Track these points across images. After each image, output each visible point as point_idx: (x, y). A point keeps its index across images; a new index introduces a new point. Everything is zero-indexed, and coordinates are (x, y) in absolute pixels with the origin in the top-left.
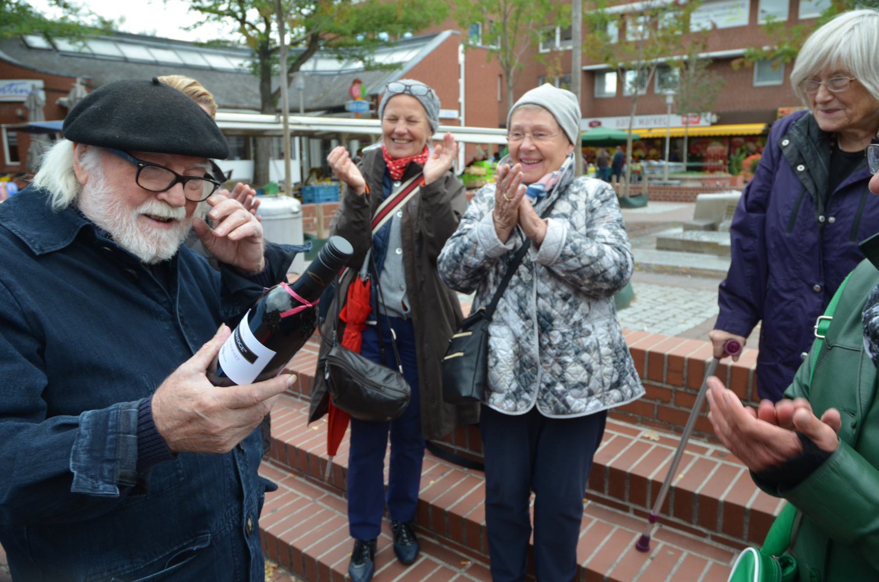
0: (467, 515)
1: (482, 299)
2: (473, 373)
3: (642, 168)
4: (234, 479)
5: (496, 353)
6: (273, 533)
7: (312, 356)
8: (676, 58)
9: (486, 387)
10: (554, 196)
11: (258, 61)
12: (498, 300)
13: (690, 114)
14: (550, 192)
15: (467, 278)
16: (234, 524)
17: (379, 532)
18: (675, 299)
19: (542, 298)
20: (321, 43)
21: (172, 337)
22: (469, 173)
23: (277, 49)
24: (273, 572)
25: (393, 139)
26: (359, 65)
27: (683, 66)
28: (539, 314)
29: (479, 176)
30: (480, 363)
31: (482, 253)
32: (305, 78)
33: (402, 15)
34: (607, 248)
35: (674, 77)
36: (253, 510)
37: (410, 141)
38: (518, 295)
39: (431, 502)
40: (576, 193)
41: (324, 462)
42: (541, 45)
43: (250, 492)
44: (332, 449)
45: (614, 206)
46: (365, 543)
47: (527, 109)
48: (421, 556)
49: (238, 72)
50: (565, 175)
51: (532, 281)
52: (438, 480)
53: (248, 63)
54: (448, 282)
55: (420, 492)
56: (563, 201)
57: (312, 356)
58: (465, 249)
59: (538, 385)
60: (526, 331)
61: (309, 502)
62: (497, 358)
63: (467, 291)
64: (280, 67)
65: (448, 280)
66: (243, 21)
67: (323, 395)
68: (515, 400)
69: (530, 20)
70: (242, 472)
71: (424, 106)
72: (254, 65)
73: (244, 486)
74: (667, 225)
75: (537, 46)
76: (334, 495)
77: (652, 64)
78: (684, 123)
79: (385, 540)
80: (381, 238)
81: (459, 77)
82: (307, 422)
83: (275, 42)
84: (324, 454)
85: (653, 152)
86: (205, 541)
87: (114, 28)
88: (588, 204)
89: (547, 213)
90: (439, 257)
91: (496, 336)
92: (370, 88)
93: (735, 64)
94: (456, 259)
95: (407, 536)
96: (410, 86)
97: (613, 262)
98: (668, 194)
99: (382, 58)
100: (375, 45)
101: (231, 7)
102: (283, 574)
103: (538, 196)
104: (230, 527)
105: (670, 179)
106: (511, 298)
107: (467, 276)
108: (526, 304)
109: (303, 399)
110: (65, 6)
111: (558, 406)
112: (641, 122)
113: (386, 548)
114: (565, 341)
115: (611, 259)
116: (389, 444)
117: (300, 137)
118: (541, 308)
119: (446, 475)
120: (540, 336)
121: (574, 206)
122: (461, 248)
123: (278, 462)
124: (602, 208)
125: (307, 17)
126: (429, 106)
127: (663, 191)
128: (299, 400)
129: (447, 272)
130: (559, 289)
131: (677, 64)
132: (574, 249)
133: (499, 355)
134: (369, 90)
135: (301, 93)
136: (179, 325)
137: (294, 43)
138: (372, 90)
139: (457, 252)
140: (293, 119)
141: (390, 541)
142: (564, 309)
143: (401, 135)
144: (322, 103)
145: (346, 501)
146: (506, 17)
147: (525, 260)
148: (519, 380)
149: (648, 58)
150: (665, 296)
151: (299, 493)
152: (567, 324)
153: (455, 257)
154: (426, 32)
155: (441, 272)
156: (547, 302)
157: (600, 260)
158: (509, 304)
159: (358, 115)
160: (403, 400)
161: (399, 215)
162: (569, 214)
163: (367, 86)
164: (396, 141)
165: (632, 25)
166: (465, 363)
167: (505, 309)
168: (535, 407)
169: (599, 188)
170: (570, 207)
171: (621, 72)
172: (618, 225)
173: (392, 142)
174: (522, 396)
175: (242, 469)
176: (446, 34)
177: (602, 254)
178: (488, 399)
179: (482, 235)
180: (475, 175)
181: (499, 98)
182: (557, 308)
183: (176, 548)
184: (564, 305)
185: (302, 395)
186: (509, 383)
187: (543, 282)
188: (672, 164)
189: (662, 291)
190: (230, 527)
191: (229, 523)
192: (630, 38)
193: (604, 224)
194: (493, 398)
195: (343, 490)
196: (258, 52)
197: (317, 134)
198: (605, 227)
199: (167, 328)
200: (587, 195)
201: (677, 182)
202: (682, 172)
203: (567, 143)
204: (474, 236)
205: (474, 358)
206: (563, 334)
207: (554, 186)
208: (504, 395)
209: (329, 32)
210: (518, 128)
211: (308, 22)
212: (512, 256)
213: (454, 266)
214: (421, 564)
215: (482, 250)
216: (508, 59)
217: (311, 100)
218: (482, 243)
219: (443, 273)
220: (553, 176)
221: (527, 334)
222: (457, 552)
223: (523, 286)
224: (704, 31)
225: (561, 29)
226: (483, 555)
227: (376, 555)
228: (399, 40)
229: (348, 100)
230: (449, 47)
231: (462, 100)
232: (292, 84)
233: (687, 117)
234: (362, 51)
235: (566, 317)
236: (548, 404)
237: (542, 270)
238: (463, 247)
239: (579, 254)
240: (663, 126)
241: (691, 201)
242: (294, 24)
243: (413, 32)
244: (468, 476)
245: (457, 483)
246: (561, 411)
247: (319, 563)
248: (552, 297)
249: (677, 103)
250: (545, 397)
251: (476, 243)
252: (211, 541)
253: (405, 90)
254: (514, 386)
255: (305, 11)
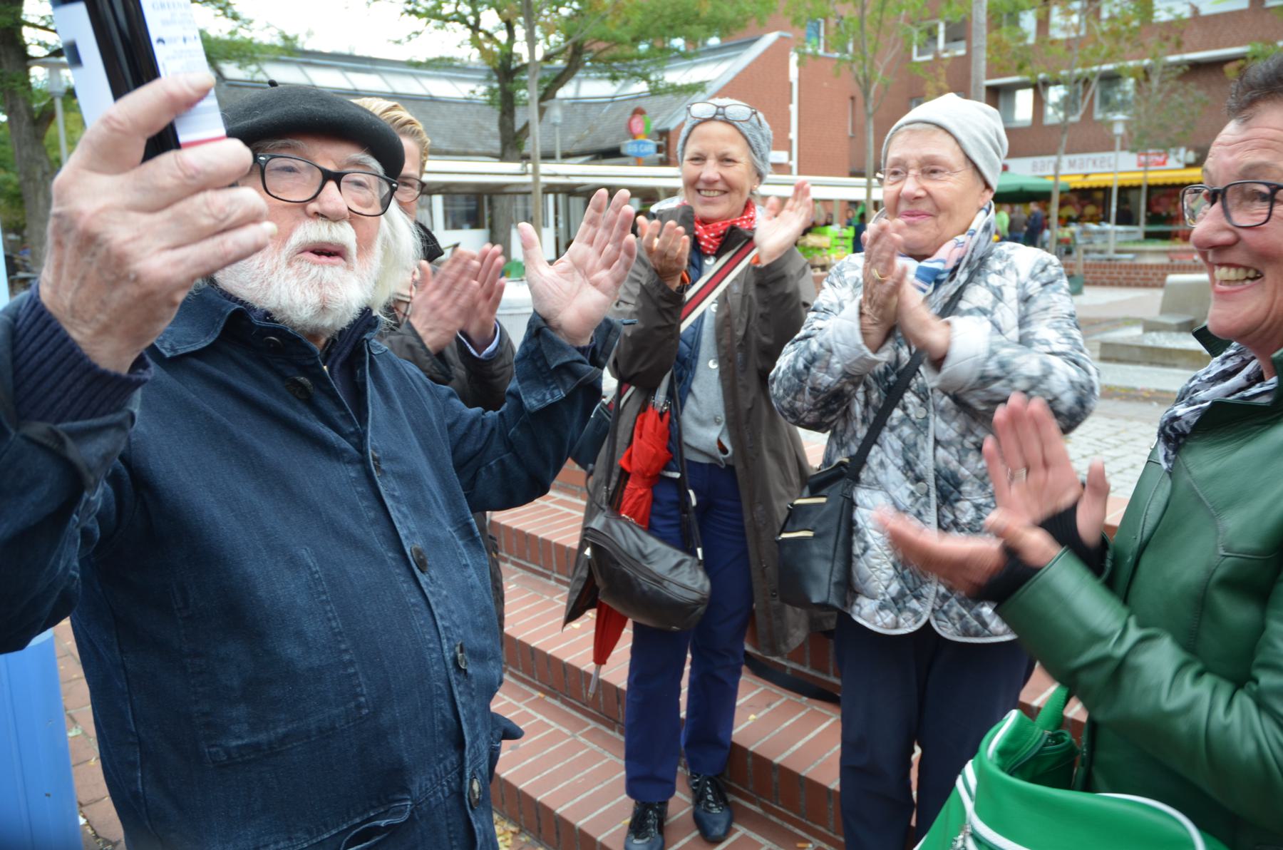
0: (807, 771)
1: (842, 445)
2: (829, 565)
3: (1073, 234)
4: (449, 715)
5: (864, 535)
6: (513, 781)
7: (572, 518)
8: (1131, 63)
9: (849, 587)
10: (962, 277)
11: (496, 85)
12: (869, 449)
13: (1150, 151)
14: (955, 269)
15: (815, 408)
16: (450, 787)
17: (672, 793)
18: (1132, 440)
19: (943, 447)
20: (586, 57)
21: (359, 489)
22: (804, 245)
23: (524, 67)
24: (512, 839)
25: (699, 191)
26: (641, 87)
27: (1141, 76)
28: (938, 474)
29: (820, 249)
30: (840, 548)
31: (838, 366)
32: (564, 108)
33: (706, 10)
34: (1056, 362)
35: (1125, 93)
36: (481, 767)
37: (725, 192)
38: (904, 442)
39: (751, 749)
40: (1000, 273)
41: (587, 676)
42: (915, 50)
43: (476, 738)
44: (602, 654)
45: (1063, 291)
46: (651, 806)
47: (912, 131)
48: (736, 831)
49: (468, 102)
50: (978, 241)
51: (926, 418)
52: (762, 714)
53: (483, 89)
54: (786, 414)
55: (735, 732)
56: (978, 287)
57: (572, 518)
58: (812, 361)
59: (934, 588)
60: (917, 500)
61: (566, 736)
62: (866, 542)
63: (816, 426)
64: (527, 94)
65: (787, 410)
66: (475, 28)
67: (583, 584)
68: (896, 610)
69: (901, 11)
70: (464, 705)
71: (746, 138)
72: (491, 91)
73: (465, 727)
74: (1115, 323)
75: (909, 51)
76: (602, 727)
77: (1094, 74)
78: (1140, 165)
79: (680, 804)
80: (687, 344)
81: (791, 102)
82: (562, 618)
83: (520, 58)
84: (589, 666)
85: (1090, 210)
86: (401, 812)
87: (299, 45)
88: (1021, 290)
89: (950, 308)
90: (772, 373)
91: (865, 506)
92: (656, 121)
93: (1230, 69)
94: (797, 375)
95: (714, 797)
96: (724, 108)
97: (1068, 385)
98: (1115, 275)
99: (676, 76)
100: (665, 56)
101: (460, 9)
102: (526, 842)
103: (935, 279)
104: (443, 792)
105: (1118, 252)
106: (892, 447)
107: (815, 405)
108: (918, 457)
109: (558, 580)
110: (235, 17)
111: (967, 622)
112: (1072, 164)
113: (681, 814)
114: (981, 518)
115: (1064, 379)
116: (689, 656)
117: (556, 193)
118: (942, 465)
119: (773, 707)
120: (938, 509)
121: (998, 294)
122: (806, 359)
123: (520, 674)
124: (1043, 295)
125: (569, 19)
126: (754, 137)
127: (1107, 270)
128: (553, 583)
129: (784, 398)
130: (972, 433)
131: (1133, 72)
132: (1002, 365)
133: (869, 539)
134: (656, 124)
135: (557, 129)
136: (370, 471)
137: (548, 58)
138: (659, 124)
139: (800, 365)
140: (545, 167)
141: (688, 805)
142: (980, 466)
143: (710, 183)
144: (587, 145)
145: (622, 739)
146: (863, 8)
147: (914, 384)
148: (903, 578)
149: (1086, 64)
150: (1117, 434)
151: (552, 723)
152: (984, 490)
153: (797, 374)
154: (739, 36)
155: (775, 396)
156: (950, 453)
157: (1046, 381)
158: (887, 456)
159: (639, 161)
160: (697, 603)
161: (714, 308)
162: (989, 308)
163: (656, 116)
164: (703, 193)
165: (1061, 14)
166: (816, 550)
167: (882, 464)
168: (928, 623)
169: (1037, 263)
170: (991, 297)
171: (1039, 89)
172: (1071, 322)
173: (697, 193)
174: (908, 605)
175: (463, 699)
176: (770, 38)
177: (1047, 372)
178: (852, 604)
179: (839, 338)
180: (812, 248)
181: (850, 133)
182: (967, 466)
183: (358, 820)
184: (979, 460)
185: (556, 575)
186: (885, 583)
187: (945, 421)
188: (1121, 228)
189: (1111, 426)
190: (443, 792)
191: (443, 786)
192: (1057, 34)
193: (1047, 321)
194: (859, 605)
195: (617, 722)
196: (495, 70)
197: (579, 189)
198: (1050, 326)
199: (353, 474)
200: (1017, 274)
201: (1130, 256)
202: (1138, 241)
203: (982, 186)
204: (827, 340)
205: (831, 541)
206: (978, 507)
207: (960, 261)
208: (877, 602)
209: (600, 39)
210: (898, 162)
211: (569, 27)
212: (892, 378)
213: (796, 388)
214: (736, 841)
215: (838, 363)
216: (867, 71)
217: (571, 140)
218: (839, 351)
219: (779, 400)
220: (957, 245)
221: (918, 506)
222: (791, 827)
223: (910, 427)
224: (1180, 20)
225: (948, 24)
226: (831, 834)
227: (665, 824)
228: (700, 48)
229: (625, 139)
230: (776, 56)
231: (793, 135)
232: (545, 117)
233: (1147, 154)
234: (646, 66)
235: (982, 478)
236: (950, 619)
237: (945, 401)
238: (810, 358)
239: (1008, 373)
240: (1107, 169)
241: (1154, 286)
242: (548, 31)
243: (721, 36)
244: (809, 709)
245: (792, 721)
246: (972, 630)
247: (580, 831)
248: (959, 447)
249: (1130, 134)
250: (945, 607)
251: (830, 351)
252: (412, 812)
253: (717, 114)
254: (895, 588)
255: (564, 11)
